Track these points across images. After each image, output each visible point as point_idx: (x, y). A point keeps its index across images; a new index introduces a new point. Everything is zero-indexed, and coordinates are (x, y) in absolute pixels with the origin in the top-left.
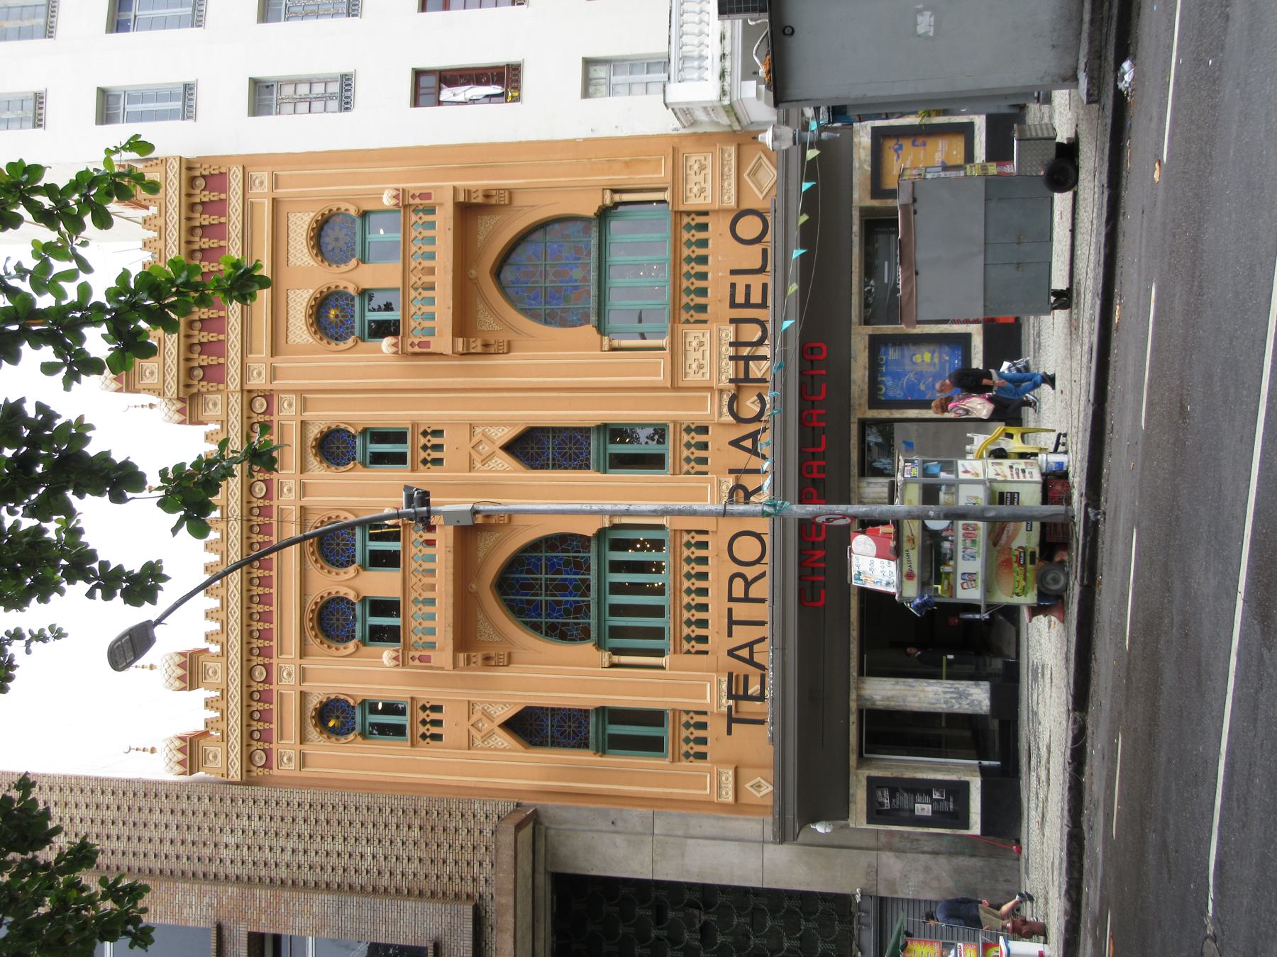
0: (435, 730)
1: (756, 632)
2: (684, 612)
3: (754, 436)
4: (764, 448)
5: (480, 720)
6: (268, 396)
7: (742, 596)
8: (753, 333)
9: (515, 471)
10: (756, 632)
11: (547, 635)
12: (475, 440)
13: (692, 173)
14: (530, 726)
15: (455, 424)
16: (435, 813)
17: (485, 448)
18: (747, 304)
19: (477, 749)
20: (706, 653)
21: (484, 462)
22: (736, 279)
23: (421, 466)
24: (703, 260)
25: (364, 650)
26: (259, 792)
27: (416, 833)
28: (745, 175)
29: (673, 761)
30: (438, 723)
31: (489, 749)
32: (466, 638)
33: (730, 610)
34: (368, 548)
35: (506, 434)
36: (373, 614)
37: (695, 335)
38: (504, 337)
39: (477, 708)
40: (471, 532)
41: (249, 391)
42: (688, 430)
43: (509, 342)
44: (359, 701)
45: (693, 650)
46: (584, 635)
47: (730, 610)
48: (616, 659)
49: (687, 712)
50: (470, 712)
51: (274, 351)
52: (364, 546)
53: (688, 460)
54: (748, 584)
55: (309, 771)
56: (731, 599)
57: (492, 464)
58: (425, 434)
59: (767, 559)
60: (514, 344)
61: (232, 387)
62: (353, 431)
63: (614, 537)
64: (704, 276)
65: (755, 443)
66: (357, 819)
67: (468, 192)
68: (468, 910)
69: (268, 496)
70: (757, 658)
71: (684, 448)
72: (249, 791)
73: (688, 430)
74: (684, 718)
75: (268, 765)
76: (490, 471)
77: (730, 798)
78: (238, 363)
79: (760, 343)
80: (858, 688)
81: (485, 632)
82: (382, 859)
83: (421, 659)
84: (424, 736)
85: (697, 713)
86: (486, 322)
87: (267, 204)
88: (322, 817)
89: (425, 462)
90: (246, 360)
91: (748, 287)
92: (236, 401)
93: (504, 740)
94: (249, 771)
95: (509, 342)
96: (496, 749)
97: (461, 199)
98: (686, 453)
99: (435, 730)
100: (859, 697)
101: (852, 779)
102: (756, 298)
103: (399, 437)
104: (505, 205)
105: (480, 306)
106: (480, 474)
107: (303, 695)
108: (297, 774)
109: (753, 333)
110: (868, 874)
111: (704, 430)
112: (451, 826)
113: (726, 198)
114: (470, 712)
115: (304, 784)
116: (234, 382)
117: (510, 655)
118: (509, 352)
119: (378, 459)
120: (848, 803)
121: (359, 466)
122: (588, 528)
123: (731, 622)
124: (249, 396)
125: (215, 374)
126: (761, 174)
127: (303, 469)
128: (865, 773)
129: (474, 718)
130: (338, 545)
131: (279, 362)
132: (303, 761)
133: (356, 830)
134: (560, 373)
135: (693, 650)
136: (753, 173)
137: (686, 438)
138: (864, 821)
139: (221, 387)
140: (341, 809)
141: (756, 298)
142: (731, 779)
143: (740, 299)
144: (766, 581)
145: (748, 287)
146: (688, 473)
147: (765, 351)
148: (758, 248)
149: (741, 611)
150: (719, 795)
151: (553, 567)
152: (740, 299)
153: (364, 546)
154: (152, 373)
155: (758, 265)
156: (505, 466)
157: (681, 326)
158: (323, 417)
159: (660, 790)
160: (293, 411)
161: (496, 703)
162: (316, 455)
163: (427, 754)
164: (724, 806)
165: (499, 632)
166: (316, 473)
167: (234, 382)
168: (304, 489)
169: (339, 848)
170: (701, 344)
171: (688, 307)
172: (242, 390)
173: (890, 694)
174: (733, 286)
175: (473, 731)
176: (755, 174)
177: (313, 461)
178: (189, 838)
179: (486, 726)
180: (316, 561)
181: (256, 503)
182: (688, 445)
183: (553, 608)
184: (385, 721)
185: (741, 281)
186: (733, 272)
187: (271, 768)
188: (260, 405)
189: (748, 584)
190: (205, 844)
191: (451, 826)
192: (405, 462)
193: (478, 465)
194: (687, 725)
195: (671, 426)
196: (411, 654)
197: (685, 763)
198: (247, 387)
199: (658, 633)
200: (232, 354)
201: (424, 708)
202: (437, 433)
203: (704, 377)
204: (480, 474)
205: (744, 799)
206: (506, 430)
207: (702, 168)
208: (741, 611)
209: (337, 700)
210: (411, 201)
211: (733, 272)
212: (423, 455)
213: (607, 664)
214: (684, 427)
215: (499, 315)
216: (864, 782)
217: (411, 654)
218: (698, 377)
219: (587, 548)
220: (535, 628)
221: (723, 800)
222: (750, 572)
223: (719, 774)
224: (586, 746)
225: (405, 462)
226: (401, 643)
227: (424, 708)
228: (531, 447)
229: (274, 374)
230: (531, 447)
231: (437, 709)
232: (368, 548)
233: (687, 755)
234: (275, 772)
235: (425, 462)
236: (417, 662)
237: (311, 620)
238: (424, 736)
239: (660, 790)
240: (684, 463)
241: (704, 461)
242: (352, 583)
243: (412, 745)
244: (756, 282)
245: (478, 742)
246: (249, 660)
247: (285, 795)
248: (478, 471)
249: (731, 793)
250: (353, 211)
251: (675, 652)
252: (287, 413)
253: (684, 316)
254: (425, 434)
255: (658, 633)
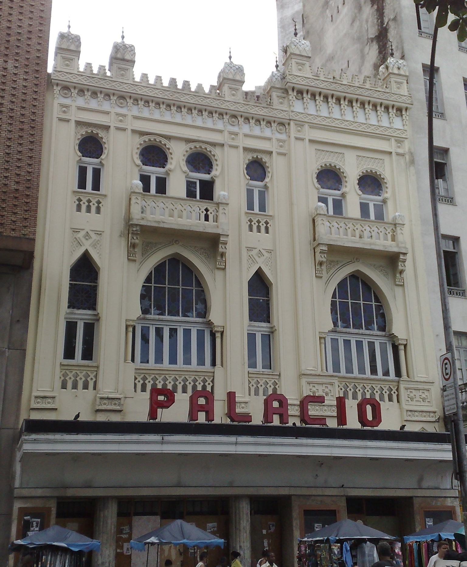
0: (84, 207)
11: (143, 286)
13: (311, 387)
20: (135, 391)
27: (13, 186)
30: (89, 210)
34: (254, 189)
36: (158, 179)
38: (325, 275)
40: (212, 244)
41: (289, 124)
43: (321, 277)
46: (145, 311)
48: (131, 329)
52: (372, 200)
64: (75, 387)
67: (404, 261)
84: (80, 200)
85: (95, 383)
94: (57, 85)
97: (402, 257)
99: (84, 207)
104: (395, 282)
112: (18, 210)
118: (128, 259)
121: (247, 182)
130: (153, 156)
133: (15, 147)
135: (136, 381)
140: (31, 140)
151: (368, 308)
153: (372, 200)
172: (290, 120)
178: (11, 39)
190: (7, 48)
191: (18, 210)
192: (79, 187)
195: (95, 364)
199: (145, 359)
209: (80, 145)
219: (199, 315)
220: (148, 280)
225: (79, 187)
227: (99, 202)
228: (260, 285)
230: (260, 285)
231: (98, 211)
232: (254, 189)
237: (155, 140)
238: (80, 200)
246: (130, 97)
250: (386, 195)
255: (145, 359)
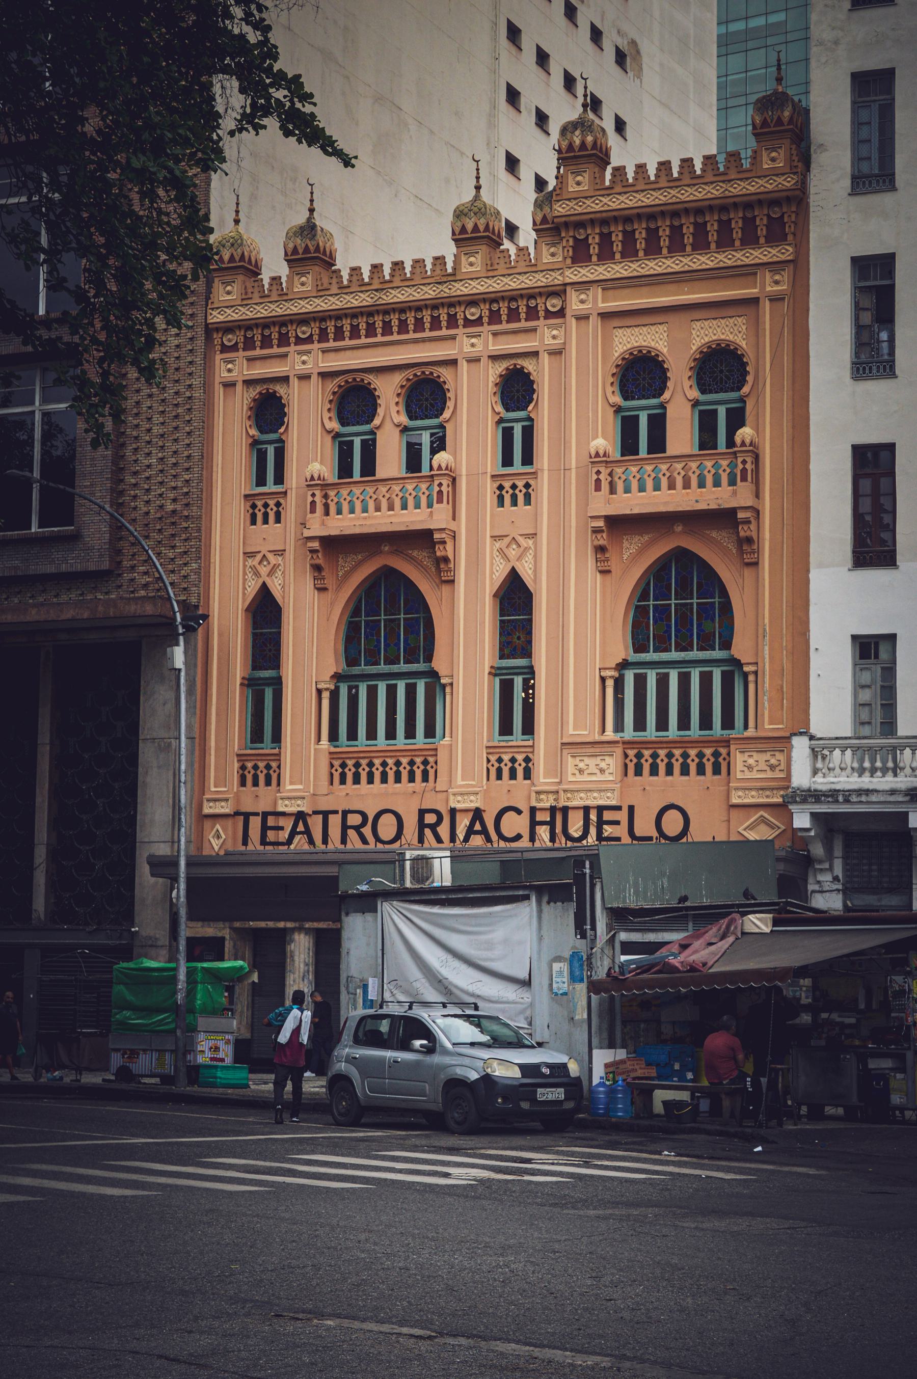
1: (318, 836)
2: (353, 761)
3: (484, 832)
4: (477, 841)
5: (269, 563)
6: (561, 313)
7: (349, 824)
8: (575, 829)
9: (492, 584)
10: (318, 836)
12: (521, 540)
14: (265, 612)
15: (536, 517)
16: (186, 526)
17: (513, 552)
18: (601, 823)
19: (245, 561)
21: (500, 551)
22: (625, 812)
23: (496, 485)
24: (685, 771)
25: (328, 439)
26: (200, 342)
27: (170, 507)
28: (762, 813)
29: (238, 755)
31: (245, 574)
32: (335, 546)
33: (336, 812)
35: (526, 572)
37: (611, 763)
39: (280, 559)
42: (527, 760)
43: (609, 572)
44: (283, 437)
45: (333, 771)
46: (352, 661)
47: (336, 812)
49: (279, 767)
50: (276, 552)
51: (605, 316)
53: (500, 760)
54: (357, 829)
55: (219, 391)
56: (345, 813)
57: (498, 559)
58: (527, 486)
59: (380, 846)
60: (608, 577)
61: (568, 273)
62: (530, 408)
63: (436, 686)
65: (477, 833)
66: (179, 447)
68: (106, 565)
69: (468, 323)
70: (297, 838)
71: (510, 756)
72: (200, 331)
73: (527, 760)
74: (274, 765)
75: (225, 349)
76: (492, 558)
77: (206, 810)
78: (592, 277)
79: (569, 837)
80: (300, 929)
81: (345, 563)
82: (147, 474)
83: (313, 503)
85: (279, 775)
86: (631, 545)
87: (753, 292)
88: (180, 410)
89: (501, 488)
90: (595, 285)
91: (617, 823)
92: (556, 279)
93: (253, 588)
95: (609, 572)
96: (245, 580)
98: (506, 758)
100: (293, 930)
101: (221, 925)
102: (608, 830)
103: (528, 459)
105: (646, 538)
106: (489, 548)
107: (285, 379)
108: (217, 380)
109: (575, 829)
110: (150, 938)
111: (527, 775)
113: (740, 793)
114: (276, 552)
115: (207, 386)
116: (571, 275)
117: (325, 589)
119: (508, 435)
120: (203, 920)
122: (439, 663)
123: (326, 814)
124: (559, 292)
125: (580, 255)
126: (763, 828)
127: (494, 358)
128: (226, 933)
129: (270, 557)
131: (594, 320)
132: (229, 385)
133: (171, 447)
134: (586, 626)
136: (763, 820)
137: (520, 758)
138: (189, 934)
139: (569, 261)
141: (608, 830)
142: (222, 811)
143: (607, 816)
144: (359, 845)
145: (617, 823)
146: (488, 761)
147: (561, 841)
148: (655, 834)
149: (335, 822)
150: (209, 800)
152: (607, 816)
154: (578, 183)
155: (638, 832)
156: (494, 574)
157: (619, 751)
158: (542, 372)
159: (213, 744)
160: (548, 341)
161: (284, 577)
162: (507, 369)
163: (239, 509)
164: (200, 806)
165: (347, 575)
166: (491, 371)
167: (571, 275)
168: (474, 360)
169: (155, 430)
170: (602, 771)
171: (639, 756)
172: (565, 285)
173: (296, 958)
174: (618, 808)
175: (259, 557)
176: (763, 821)
177: (501, 368)
179: (264, 570)
180: (408, 380)
181: (459, 310)
182: (513, 760)
183: (373, 627)
184: (268, 462)
185: (623, 816)
186: (631, 809)
187: (222, 352)
188: (553, 304)
189: (357, 829)
193: (498, 545)
194: (268, 767)
196: (318, 493)
197: (236, 765)
198: (568, 289)
200: (600, 269)
201: (278, 504)
202: (528, 499)
203: (571, 776)
204: (489, 548)
205: (207, 824)
206: (530, 572)
207: (772, 768)
208: (335, 822)
210: (740, 460)
211: (631, 809)
212: (507, 485)
213: (319, 686)
214: (530, 755)
215: (636, 559)
216: (220, 934)
217: (318, 493)
218: (571, 769)
221: (205, 803)
222: (367, 831)
223: (227, 800)
224: (254, 668)
226: (337, 481)
228: (515, 598)
229: (582, 318)
230: (515, 598)
233: (243, 768)
234: (218, 357)
235: (501, 488)
236: (310, 499)
238: (254, 506)
239: (213, 744)
240: (497, 756)
241: (499, 777)
242: (388, 419)
243: (246, 496)
244: (621, 831)
245: (250, 562)
247: (197, 369)
248: (492, 545)
249: (211, 811)
251: (330, 753)
252: (547, 335)
253: (631, 753)
254: (527, 486)
